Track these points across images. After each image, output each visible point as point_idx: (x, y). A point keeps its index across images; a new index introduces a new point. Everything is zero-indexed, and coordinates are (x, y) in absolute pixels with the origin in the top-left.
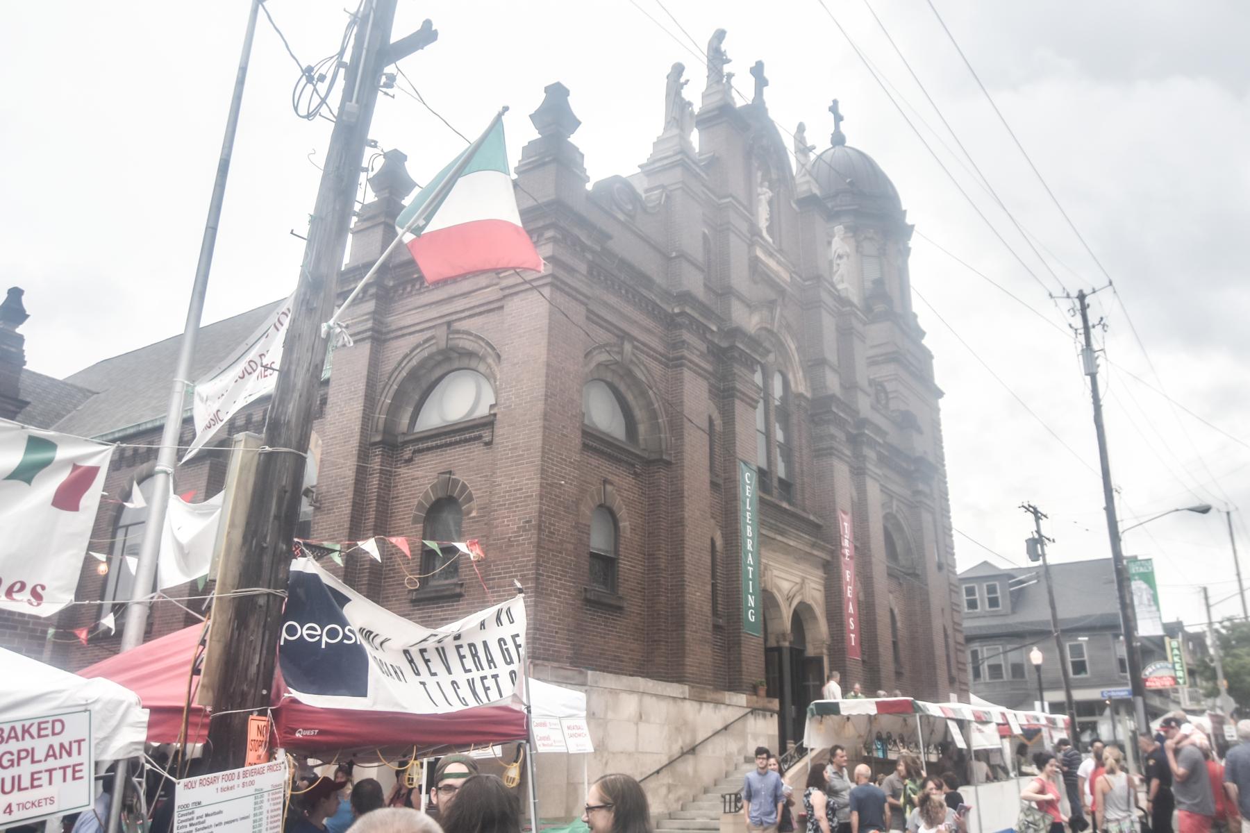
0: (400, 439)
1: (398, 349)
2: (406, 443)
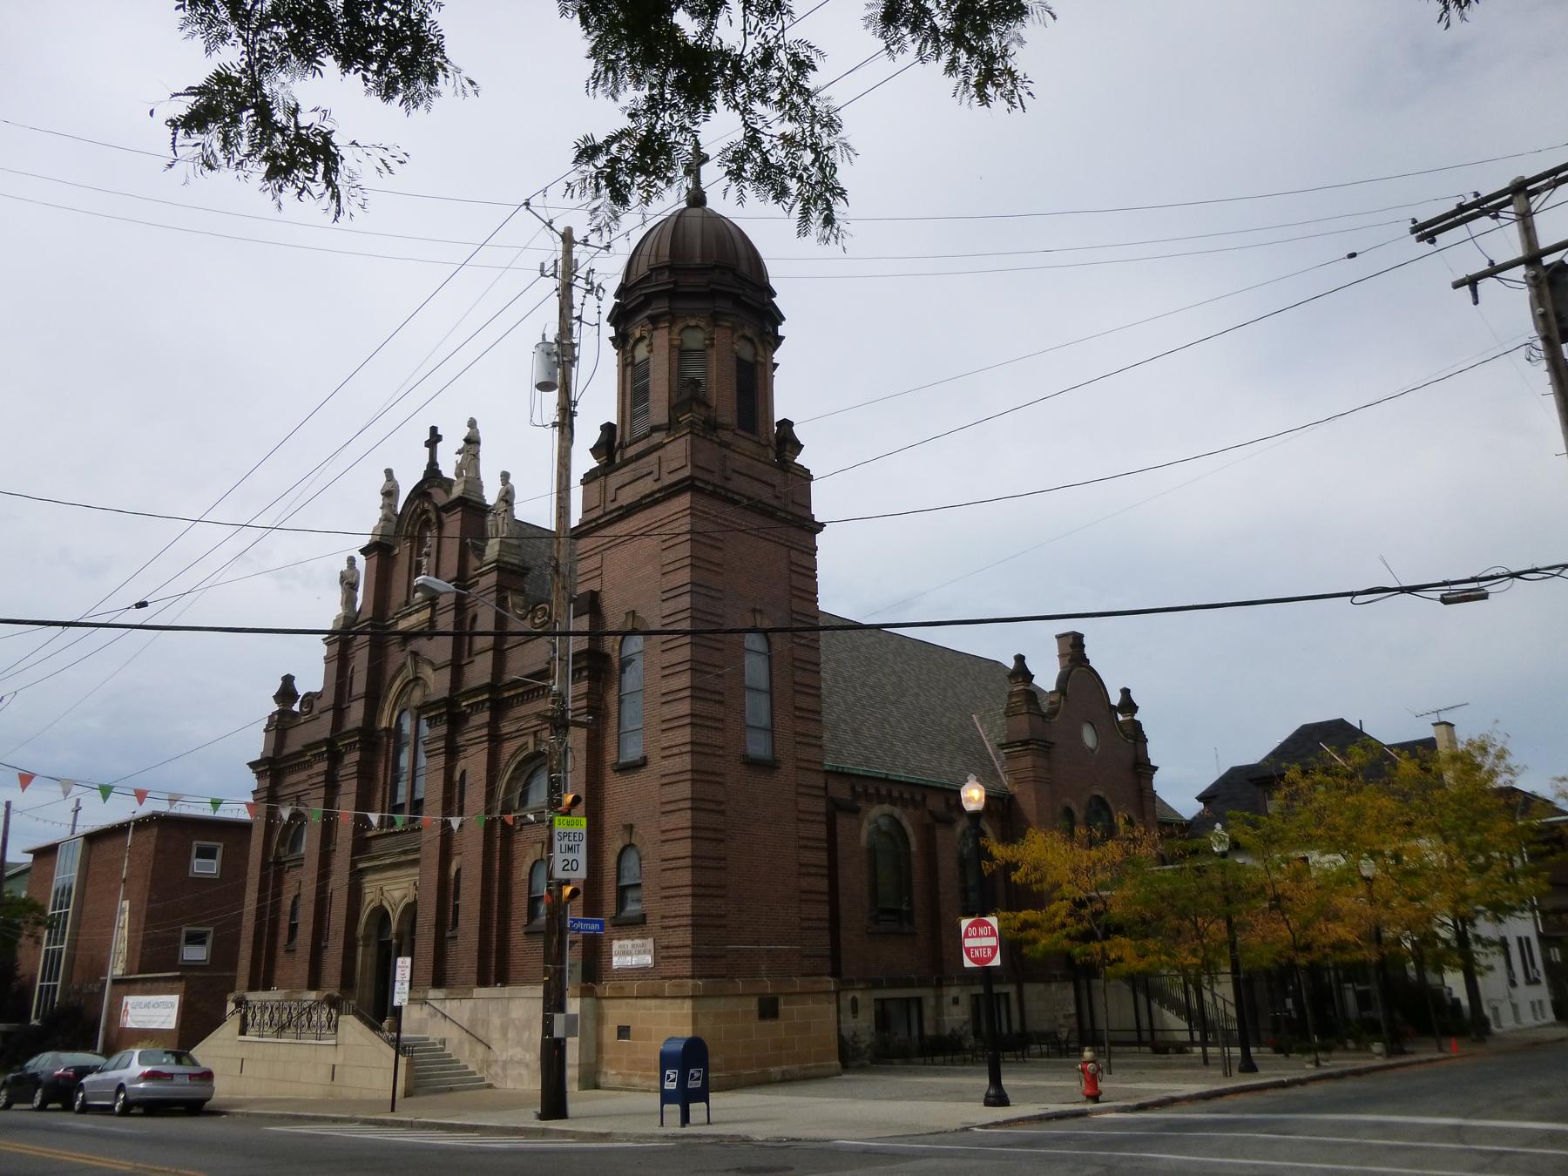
0: (283, 859)
1: (509, 748)
2: (285, 862)
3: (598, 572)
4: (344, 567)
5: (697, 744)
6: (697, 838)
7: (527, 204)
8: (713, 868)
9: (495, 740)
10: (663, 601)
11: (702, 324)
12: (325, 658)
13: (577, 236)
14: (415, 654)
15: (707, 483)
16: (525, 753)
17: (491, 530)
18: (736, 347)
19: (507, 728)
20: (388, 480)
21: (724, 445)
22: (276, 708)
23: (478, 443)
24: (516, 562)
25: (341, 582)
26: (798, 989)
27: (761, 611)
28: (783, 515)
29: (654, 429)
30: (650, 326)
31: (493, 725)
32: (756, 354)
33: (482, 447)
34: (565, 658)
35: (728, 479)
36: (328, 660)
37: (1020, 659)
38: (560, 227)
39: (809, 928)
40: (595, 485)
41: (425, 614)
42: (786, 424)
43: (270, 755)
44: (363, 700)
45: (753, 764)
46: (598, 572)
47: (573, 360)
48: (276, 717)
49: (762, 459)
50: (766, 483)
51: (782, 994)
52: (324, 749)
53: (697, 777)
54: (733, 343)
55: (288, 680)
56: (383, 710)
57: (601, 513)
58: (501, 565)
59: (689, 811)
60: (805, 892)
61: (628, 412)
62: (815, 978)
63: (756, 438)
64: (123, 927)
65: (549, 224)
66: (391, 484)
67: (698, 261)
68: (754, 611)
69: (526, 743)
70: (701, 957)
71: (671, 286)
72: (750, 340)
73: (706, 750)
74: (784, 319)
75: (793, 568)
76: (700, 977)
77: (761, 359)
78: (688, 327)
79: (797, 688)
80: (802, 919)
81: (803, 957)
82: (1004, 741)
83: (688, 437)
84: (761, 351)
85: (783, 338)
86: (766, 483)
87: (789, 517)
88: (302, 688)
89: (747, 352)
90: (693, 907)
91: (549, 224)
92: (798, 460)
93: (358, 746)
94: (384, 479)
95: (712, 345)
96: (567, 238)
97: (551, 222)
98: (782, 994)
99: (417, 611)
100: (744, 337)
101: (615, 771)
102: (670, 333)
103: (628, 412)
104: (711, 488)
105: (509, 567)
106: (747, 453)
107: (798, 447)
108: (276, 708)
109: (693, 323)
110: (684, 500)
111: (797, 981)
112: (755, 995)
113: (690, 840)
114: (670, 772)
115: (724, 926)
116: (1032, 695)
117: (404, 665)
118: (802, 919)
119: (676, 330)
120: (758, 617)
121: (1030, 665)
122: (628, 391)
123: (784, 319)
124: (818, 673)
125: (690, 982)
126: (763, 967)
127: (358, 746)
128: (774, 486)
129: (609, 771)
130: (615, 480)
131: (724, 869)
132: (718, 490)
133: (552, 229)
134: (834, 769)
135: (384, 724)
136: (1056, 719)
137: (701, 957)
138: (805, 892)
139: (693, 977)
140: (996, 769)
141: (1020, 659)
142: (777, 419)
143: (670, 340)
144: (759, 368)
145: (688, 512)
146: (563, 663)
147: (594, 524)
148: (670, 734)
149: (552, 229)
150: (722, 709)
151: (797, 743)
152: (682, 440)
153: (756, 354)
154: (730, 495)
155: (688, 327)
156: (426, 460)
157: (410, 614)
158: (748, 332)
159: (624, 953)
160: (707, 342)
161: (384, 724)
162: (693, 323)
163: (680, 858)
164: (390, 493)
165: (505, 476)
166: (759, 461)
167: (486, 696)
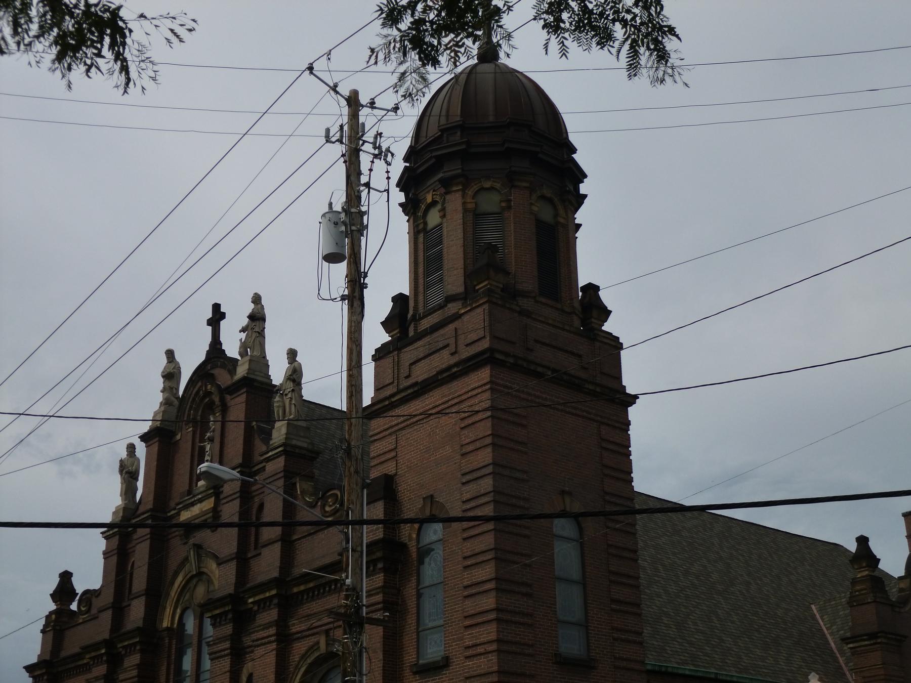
1: (299, 648)
3: (393, 454)
4: (124, 454)
7: (310, 69)
9: (284, 640)
10: (463, 484)
12: (105, 553)
13: (364, 99)
14: (198, 547)
15: (507, 355)
16: (316, 654)
17: (277, 411)
18: (535, 208)
19: (296, 627)
20: (169, 362)
21: (523, 313)
22: (53, 607)
23: (263, 319)
24: (305, 445)
25: (121, 472)
27: (570, 493)
28: (591, 387)
29: (450, 299)
30: (443, 190)
31: (282, 624)
32: (556, 215)
33: (268, 324)
34: (359, 549)
35: (532, 350)
36: (106, 554)
37: (863, 541)
38: (345, 90)
40: (388, 361)
41: (208, 504)
42: (592, 289)
43: (48, 657)
44: (143, 598)
45: (564, 663)
46: (393, 454)
47: (362, 229)
48: (53, 616)
49: (567, 327)
50: (572, 353)
52: (103, 651)
54: (532, 204)
55: (66, 577)
56: (165, 608)
57: (395, 390)
58: (288, 449)
61: (421, 281)
65: (334, 88)
66: (172, 366)
67: (491, 119)
68: (563, 493)
69: (318, 643)
71: (464, 147)
72: (550, 201)
77: (562, 220)
78: (483, 189)
82: (848, 635)
83: (486, 306)
84: (562, 212)
85: (585, 196)
86: (572, 353)
87: (598, 390)
88: (80, 587)
89: (546, 214)
91: (334, 88)
92: (607, 327)
93: (138, 648)
94: (164, 360)
96: (353, 101)
97: (336, 86)
99: (200, 501)
100: (543, 197)
101: (415, 673)
102: (463, 197)
103: (421, 281)
104: (511, 360)
105: (297, 451)
106: (550, 322)
107: (605, 313)
108: (53, 607)
109: (487, 184)
110: (484, 375)
114: (475, 673)
116: (879, 580)
117: (186, 559)
119: (470, 193)
120: (568, 500)
121: (875, 547)
122: (421, 259)
127: (138, 648)
128: (580, 356)
129: (407, 673)
130: (409, 354)
133: (337, 93)
134: (657, 668)
135: (165, 624)
136: (907, 609)
140: (840, 667)
141: (863, 541)
142: (582, 282)
143: (464, 203)
145: (488, 387)
146: (357, 555)
147: (387, 403)
148: (475, 631)
149: (337, 93)
151: (615, 639)
152: (479, 310)
153: (556, 215)
154: (533, 367)
155: (483, 189)
156: (209, 339)
157: (193, 504)
158: (547, 192)
160: (503, 204)
161: (165, 624)
162: (487, 184)
164: (171, 376)
165: (292, 354)
166: (563, 329)
167: (274, 592)
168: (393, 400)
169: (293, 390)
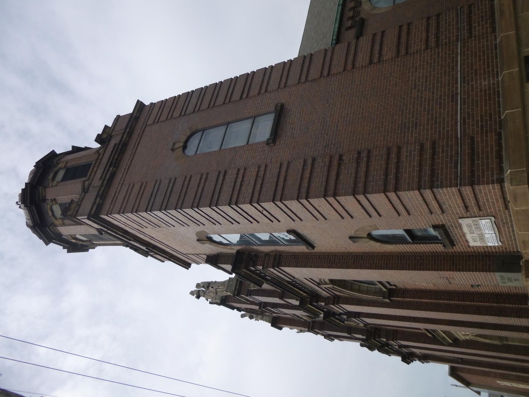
5: (420, 181)
6: (308, 192)
8: (368, 167)
11: (49, 207)
26: (513, 33)
32: (61, 168)
39: (437, 38)
51: (519, 52)
53: (391, 186)
59: (474, 186)
60: (398, 52)
62: (497, 14)
63: (94, 162)
64: (512, 384)
70: (472, 172)
73: (258, 186)
74: (53, 151)
75: (325, 73)
76: (501, 170)
79: (403, 51)
80: (427, 48)
81: (470, 36)
90: (410, 189)
95: (55, 200)
98: (519, 52)
104: (98, 199)
105: (237, 288)
111: (500, 36)
112: (522, 87)
113: (477, 187)
115: (434, 143)
118: (427, 48)
123: (53, 151)
124: (312, 55)
125: (507, 185)
126: (485, 83)
131: (369, 152)
132: (101, 193)
137: (472, 172)
138: (398, 52)
139: (501, 181)
144: (69, 164)
150: (229, 172)
159: (482, 237)
163: (147, 222)
168: (168, 257)
169: (212, 287)
